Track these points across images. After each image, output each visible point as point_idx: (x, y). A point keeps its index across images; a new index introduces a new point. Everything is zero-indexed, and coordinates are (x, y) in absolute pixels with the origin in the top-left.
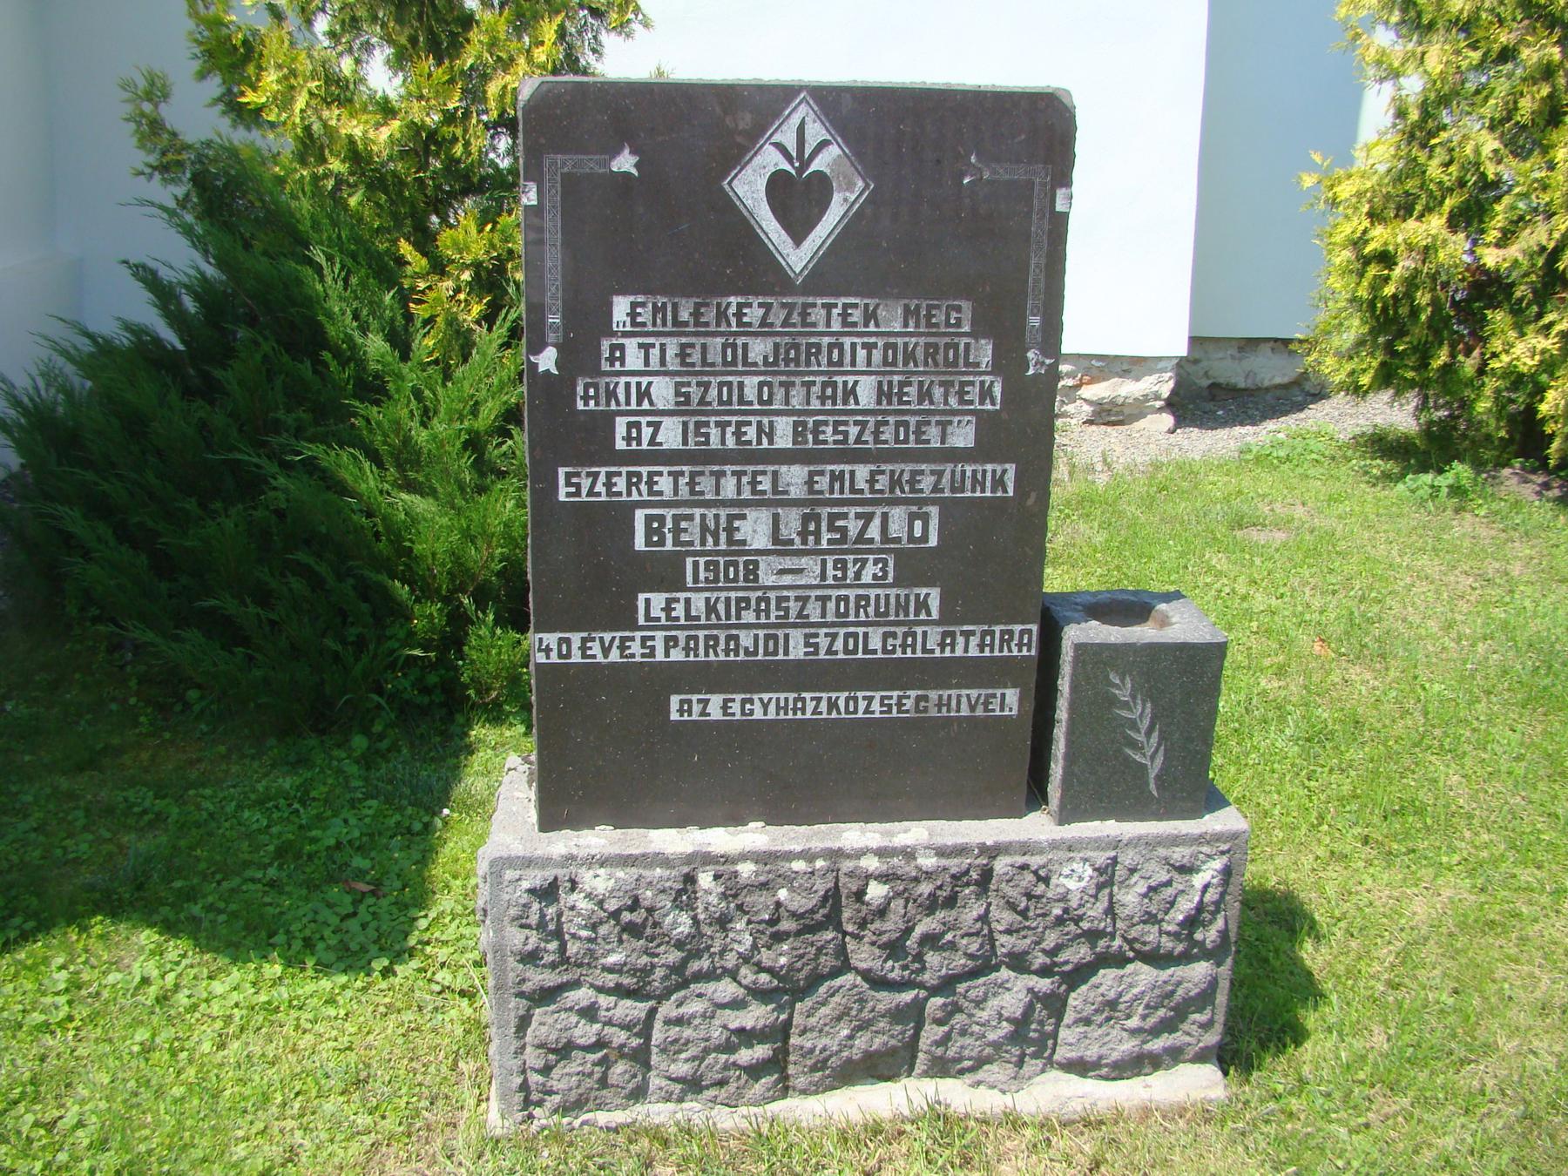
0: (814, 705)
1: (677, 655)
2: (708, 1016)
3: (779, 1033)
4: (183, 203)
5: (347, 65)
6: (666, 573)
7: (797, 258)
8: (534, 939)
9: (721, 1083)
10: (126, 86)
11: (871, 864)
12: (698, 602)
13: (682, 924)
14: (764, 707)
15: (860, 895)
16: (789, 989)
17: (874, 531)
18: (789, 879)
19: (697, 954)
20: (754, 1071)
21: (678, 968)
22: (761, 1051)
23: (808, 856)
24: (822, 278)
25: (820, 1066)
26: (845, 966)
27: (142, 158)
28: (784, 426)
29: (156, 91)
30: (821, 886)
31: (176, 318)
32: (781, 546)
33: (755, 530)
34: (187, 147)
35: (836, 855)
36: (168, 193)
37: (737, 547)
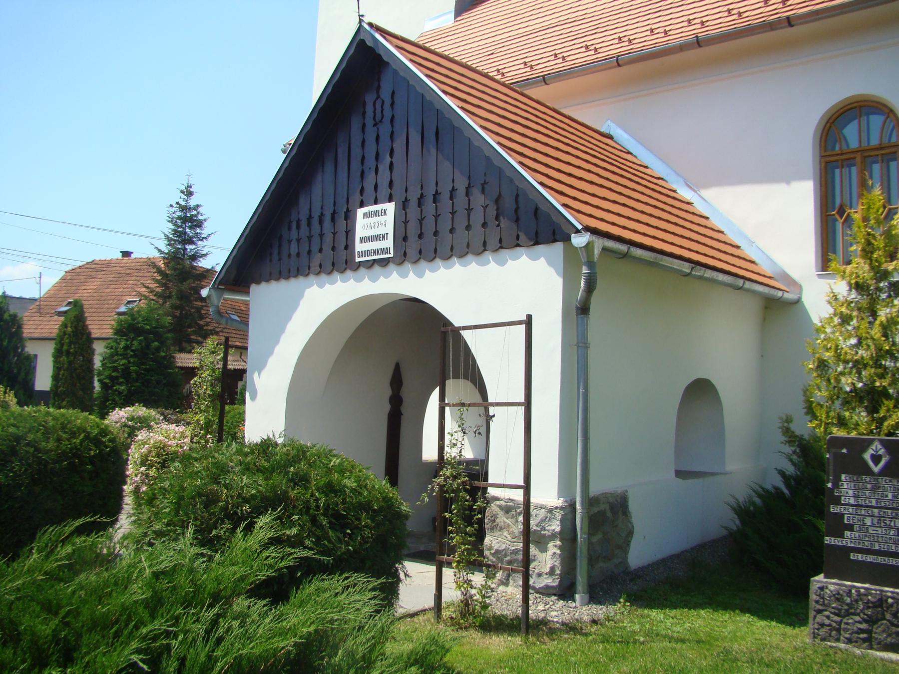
0: (880, 560)
1: (852, 545)
2: (853, 624)
3: (869, 632)
4: (794, 452)
5: (847, 414)
6: (850, 528)
7: (876, 469)
8: (818, 598)
9: (856, 642)
10: (781, 418)
11: (890, 594)
12: (857, 534)
13: (848, 600)
14: (870, 558)
15: (886, 601)
16: (871, 621)
17: (892, 524)
18: (871, 594)
19: (851, 608)
20: (864, 640)
21: (847, 610)
22: (865, 635)
23: (876, 590)
24: (882, 473)
25: (879, 643)
26: (884, 619)
27: (783, 439)
28: (874, 501)
29: (789, 420)
30: (878, 597)
31: (788, 485)
32: (873, 525)
33: (868, 521)
34: (796, 436)
35: (882, 591)
36: (788, 449)
37: (865, 524)
